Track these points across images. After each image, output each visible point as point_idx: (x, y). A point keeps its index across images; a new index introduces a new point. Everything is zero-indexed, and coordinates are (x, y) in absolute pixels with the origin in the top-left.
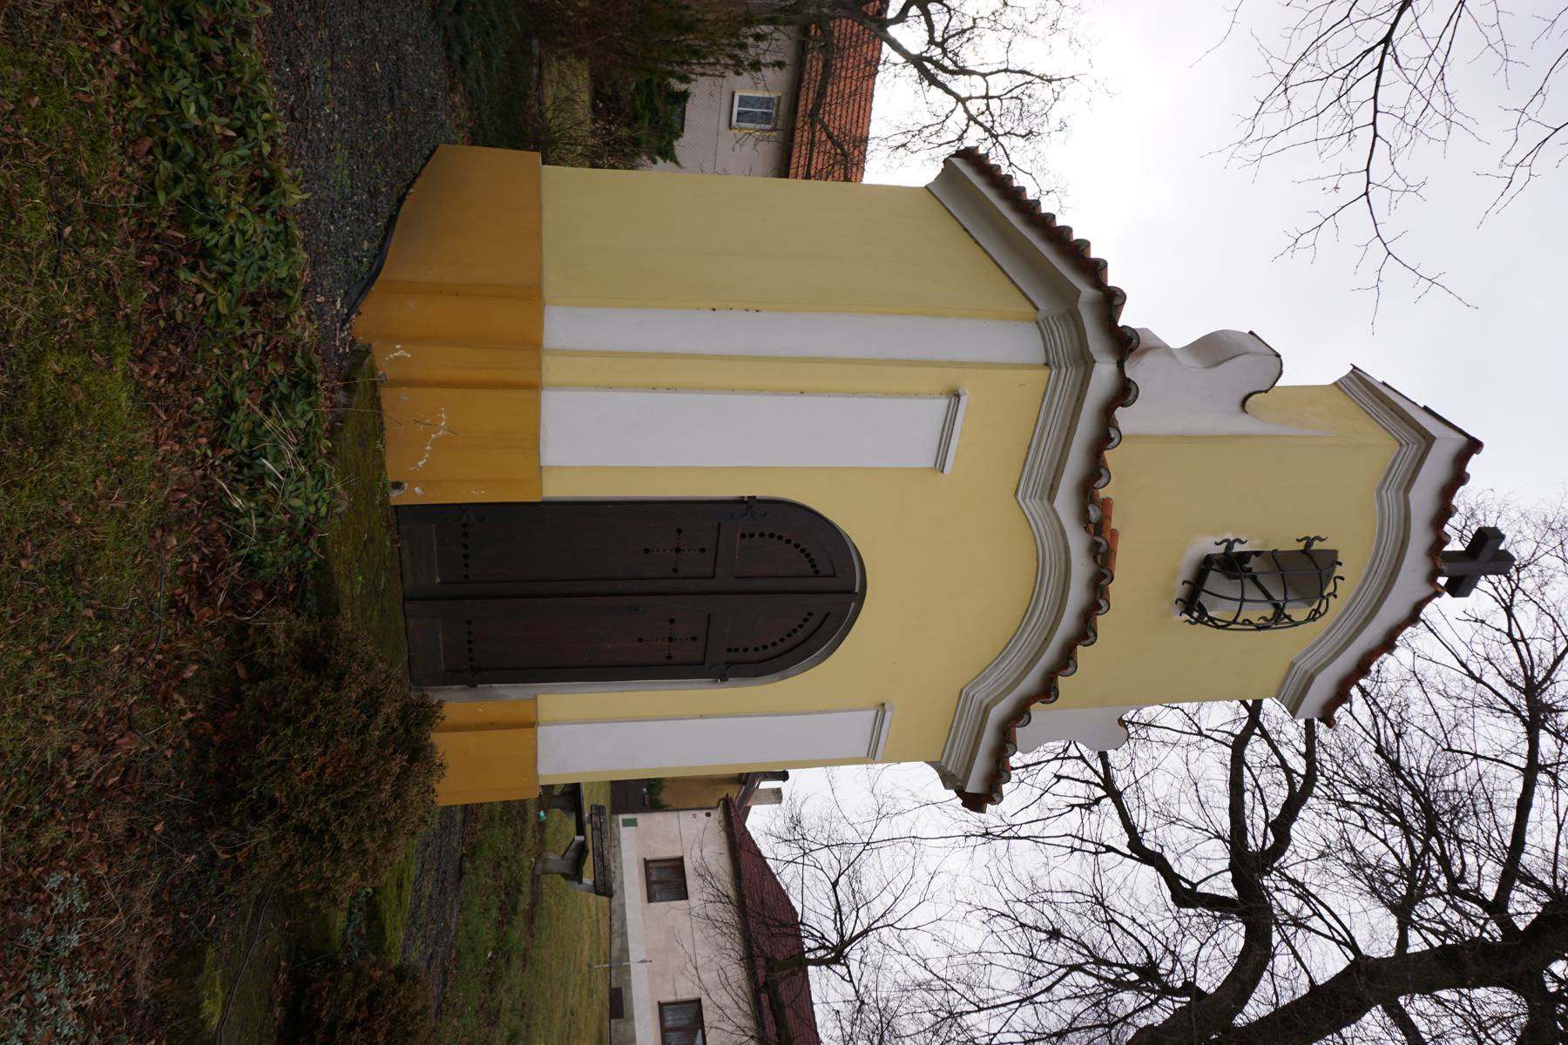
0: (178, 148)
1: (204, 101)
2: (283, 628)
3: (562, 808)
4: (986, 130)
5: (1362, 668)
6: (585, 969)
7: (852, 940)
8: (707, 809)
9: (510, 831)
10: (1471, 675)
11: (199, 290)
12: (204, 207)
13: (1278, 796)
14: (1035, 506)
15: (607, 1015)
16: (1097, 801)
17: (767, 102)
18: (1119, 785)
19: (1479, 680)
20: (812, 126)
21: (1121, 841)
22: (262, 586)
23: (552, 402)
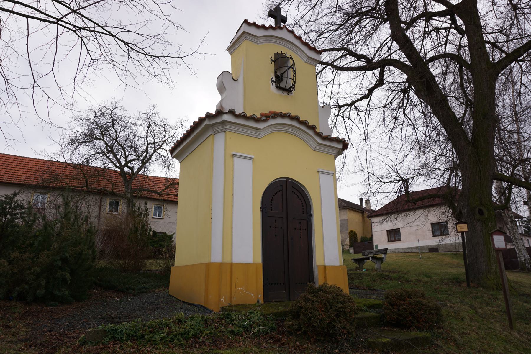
0: (171, 338)
1: (161, 332)
2: (288, 322)
3: (363, 264)
4: (164, 143)
5: (306, 44)
6: (421, 260)
7: (401, 177)
8: (371, 223)
9: (364, 277)
10: (315, 6)
11: (204, 337)
12: (185, 334)
13: (350, 58)
14: (262, 133)
15: (437, 253)
16: (356, 108)
17: (155, 208)
18: (351, 101)
19: (316, 4)
20: (163, 194)
21: (366, 101)
22: (279, 328)
23: (237, 259)
